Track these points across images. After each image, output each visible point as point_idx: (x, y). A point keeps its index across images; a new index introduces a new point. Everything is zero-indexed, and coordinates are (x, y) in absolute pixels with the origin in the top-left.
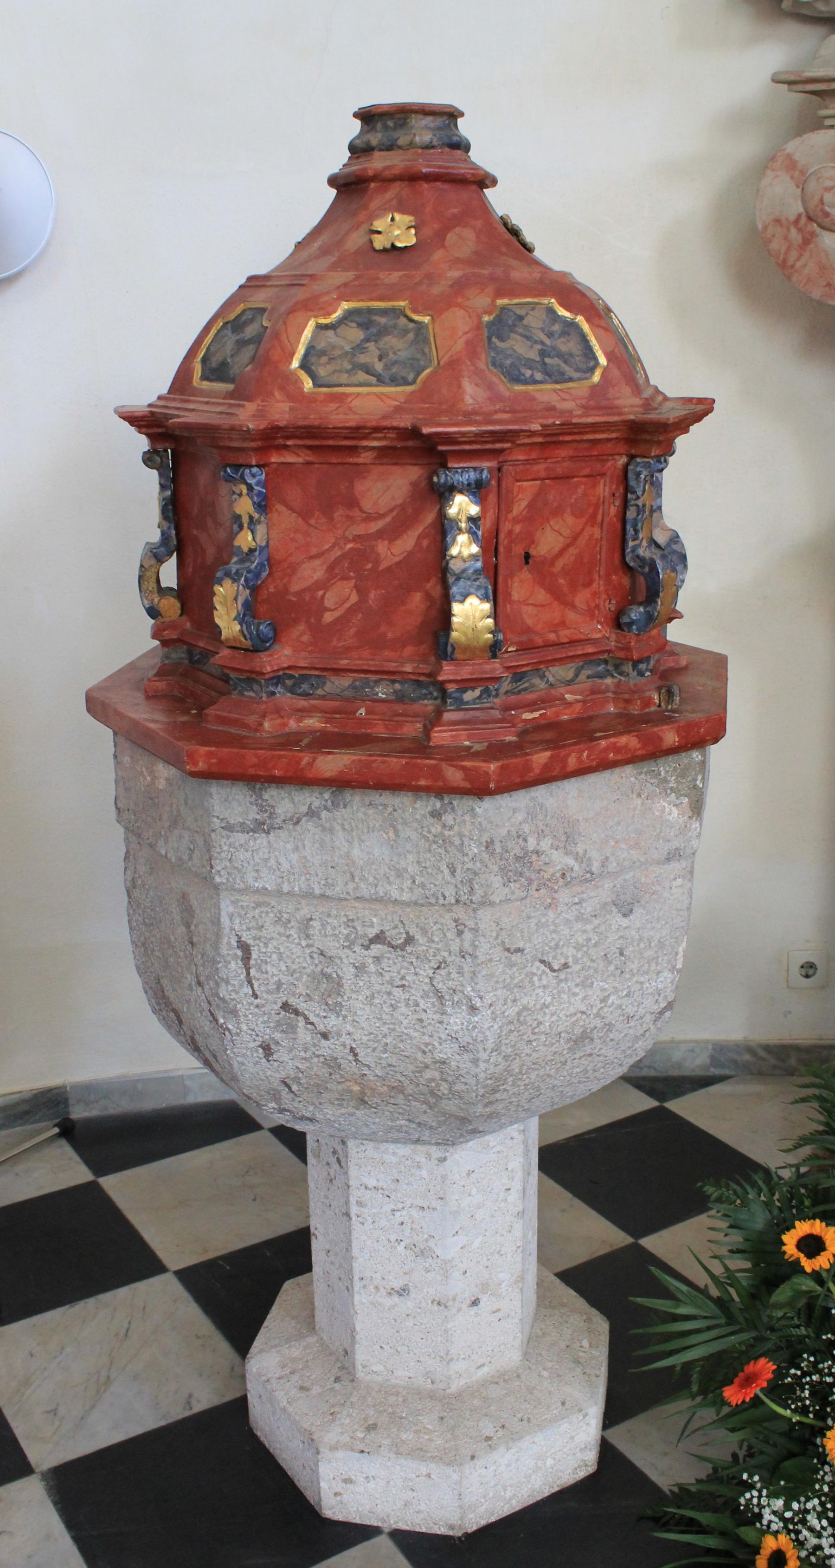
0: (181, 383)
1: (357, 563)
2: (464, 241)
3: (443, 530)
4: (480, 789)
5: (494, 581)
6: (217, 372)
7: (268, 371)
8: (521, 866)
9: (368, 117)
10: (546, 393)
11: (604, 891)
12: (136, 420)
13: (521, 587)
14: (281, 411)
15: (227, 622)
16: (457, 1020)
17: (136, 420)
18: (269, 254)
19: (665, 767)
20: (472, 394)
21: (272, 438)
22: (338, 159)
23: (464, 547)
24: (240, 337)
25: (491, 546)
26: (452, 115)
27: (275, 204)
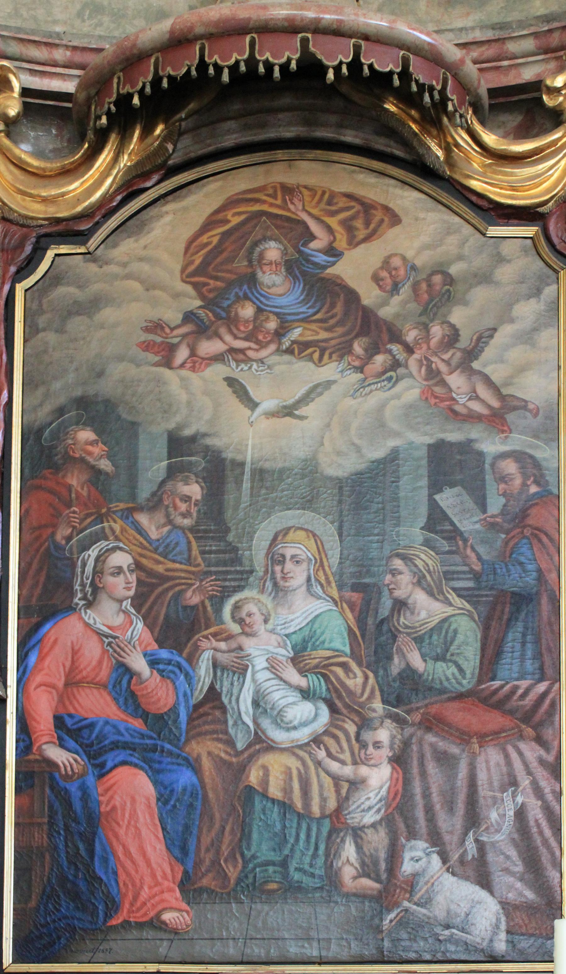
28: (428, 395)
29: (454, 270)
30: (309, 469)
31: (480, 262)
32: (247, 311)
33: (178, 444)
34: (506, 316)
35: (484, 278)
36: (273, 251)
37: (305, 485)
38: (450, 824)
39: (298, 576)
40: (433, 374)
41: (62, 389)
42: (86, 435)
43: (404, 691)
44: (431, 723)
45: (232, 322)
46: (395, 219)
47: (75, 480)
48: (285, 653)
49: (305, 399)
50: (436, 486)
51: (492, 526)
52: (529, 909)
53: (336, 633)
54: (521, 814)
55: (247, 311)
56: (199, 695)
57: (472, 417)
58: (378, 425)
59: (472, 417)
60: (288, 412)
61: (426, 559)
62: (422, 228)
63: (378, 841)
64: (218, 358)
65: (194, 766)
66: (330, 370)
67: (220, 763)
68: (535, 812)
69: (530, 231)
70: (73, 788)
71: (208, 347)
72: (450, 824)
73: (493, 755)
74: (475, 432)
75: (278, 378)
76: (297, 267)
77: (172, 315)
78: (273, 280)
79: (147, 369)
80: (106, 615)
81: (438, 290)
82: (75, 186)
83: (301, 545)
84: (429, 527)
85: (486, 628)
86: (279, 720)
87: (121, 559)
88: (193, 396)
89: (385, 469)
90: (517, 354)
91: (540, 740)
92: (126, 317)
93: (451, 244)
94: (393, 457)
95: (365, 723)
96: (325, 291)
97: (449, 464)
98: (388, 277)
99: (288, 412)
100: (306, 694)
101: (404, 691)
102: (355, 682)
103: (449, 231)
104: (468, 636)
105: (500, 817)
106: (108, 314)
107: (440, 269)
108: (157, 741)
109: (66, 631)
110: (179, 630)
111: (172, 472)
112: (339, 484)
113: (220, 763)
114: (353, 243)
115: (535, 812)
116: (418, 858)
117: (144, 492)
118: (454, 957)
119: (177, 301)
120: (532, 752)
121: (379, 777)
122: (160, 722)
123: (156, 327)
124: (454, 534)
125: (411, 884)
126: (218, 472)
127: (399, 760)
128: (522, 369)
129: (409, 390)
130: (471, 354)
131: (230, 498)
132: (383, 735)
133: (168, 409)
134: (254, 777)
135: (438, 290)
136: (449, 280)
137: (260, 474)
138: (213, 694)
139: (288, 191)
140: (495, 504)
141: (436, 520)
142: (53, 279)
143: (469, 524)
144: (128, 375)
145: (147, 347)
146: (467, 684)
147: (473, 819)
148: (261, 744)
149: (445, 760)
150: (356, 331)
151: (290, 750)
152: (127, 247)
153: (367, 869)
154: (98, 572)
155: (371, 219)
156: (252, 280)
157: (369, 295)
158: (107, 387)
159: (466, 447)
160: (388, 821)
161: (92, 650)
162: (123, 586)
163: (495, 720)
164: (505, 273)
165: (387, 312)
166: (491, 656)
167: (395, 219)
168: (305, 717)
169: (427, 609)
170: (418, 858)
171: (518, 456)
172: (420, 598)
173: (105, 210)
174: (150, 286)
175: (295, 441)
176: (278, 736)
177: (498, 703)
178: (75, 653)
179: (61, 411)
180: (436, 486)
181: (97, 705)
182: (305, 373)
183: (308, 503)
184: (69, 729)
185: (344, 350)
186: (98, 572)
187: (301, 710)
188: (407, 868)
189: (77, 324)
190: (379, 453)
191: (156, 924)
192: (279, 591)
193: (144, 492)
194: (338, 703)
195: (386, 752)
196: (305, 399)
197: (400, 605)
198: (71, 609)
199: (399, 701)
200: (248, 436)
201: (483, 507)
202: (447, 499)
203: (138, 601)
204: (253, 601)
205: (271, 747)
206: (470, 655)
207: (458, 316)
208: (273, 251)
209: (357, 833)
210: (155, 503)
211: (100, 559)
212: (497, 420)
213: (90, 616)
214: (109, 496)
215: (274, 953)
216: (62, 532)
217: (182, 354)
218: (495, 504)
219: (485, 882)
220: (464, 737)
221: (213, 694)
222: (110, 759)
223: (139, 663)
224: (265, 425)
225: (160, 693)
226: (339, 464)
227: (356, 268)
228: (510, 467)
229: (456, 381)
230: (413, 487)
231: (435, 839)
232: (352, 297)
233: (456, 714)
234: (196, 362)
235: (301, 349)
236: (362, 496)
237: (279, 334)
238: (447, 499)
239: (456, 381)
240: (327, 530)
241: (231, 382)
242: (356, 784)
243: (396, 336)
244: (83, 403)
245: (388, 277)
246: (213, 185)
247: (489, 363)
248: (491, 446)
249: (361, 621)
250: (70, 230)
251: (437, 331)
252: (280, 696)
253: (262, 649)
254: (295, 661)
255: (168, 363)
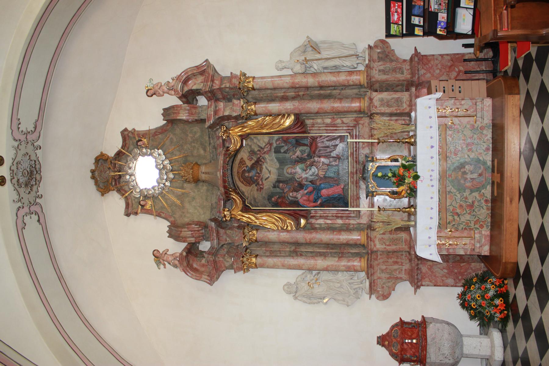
0: (397, 360)
1: (411, 349)
2: (387, 338)
3: (408, 342)
4: (426, 342)
5: (412, 339)
6: (396, 357)
7: (397, 354)
8: (434, 339)
9: (378, 344)
10: (399, 334)
11: (437, 331)
12: (423, 316)
13: (413, 337)
14: (399, 353)
15: (415, 359)
16: (446, 344)
17: (423, 316)
18: (387, 353)
19: (427, 326)
20: (399, 340)
21: (401, 354)
22: (380, 346)
23: (410, 341)
24: (393, 355)
25: (410, 339)
26: (378, 337)
27: (383, 352)
28: (267, 154)
29: (249, 150)
30: (278, 169)
31: (248, 147)
32: (255, 178)
33: (274, 187)
34: (256, 144)
35: (250, 146)
36: (247, 174)
37: (280, 169)
38: (329, 150)
39: (293, 171)
40: (264, 153)
41: (266, 202)
42: (273, 199)
43: (310, 156)
44: (314, 152)
45: (257, 180)
46: (242, 158)
47: (280, 200)
48: (304, 172)
49: (268, 170)
50: (280, 152)
51: (286, 145)
52: (341, 140)
53: (302, 166)
54: (327, 141)
55: (255, 178)
56: (310, 183)
57: (271, 148)
58: (272, 160)
59: (271, 148)
60: (270, 172)
61: (291, 154)
62: (244, 155)
63: (331, 159)
64: (262, 182)
65: (320, 184)
66: (264, 167)
67: (320, 181)
68: (327, 139)
69: (244, 141)
70: (324, 200)
71: (260, 183)
72: (329, 150)
73: (319, 144)
74: (273, 148)
75: (265, 173)
76: (249, 171)
77: (256, 188)
78: (251, 175)
79: (264, 191)
80: (299, 196)
81: (252, 152)
82: (238, 201)
83: (288, 170)
84: (286, 153)
85: (301, 146)
86: (314, 173)
87: (291, 194)
88: (267, 185)
89: (278, 159)
90: (261, 142)
91: (317, 138)
92: (256, 194)
93: (246, 151)
94: (276, 158)
95: (314, 162)
96: (253, 167)
97: (277, 151)
98: (251, 159)
99: (270, 172)
100: (310, 169)
101: (310, 156)
102: (309, 163)
103: (244, 151)
104: (301, 148)
105: (328, 143)
106: (256, 196)
107: (249, 152)
108: (317, 189)
109: (301, 201)
110: (301, 186)
111: (278, 187)
112: (280, 165)
113: (320, 181)
114: (245, 164)
115: (327, 139)
116: (333, 154)
117: (281, 191)
118: (401, 29)
119: (254, 187)
120: (318, 139)
121: (322, 159)
122: (314, 189)
123: (257, 190)
124: (287, 150)
125: (337, 155)
126: (279, 181)
127: (320, 157)
128: (264, 141)
129: (267, 156)
130: (261, 148)
131: (282, 180)
132: (316, 159)
133: (269, 188)
134: (322, 176)
135: (252, 152)
136: (251, 151)
137: (279, 176)
138: (310, 182)
139: (238, 173)
140: (283, 144)
141: (285, 152)
142: (251, 204)
143: (286, 148)
144: (264, 193)
145: (260, 191)
146: (309, 148)
147: (328, 147)
148: (317, 175)
149: (320, 151)
150: (258, 163)
151: (318, 171)
152: (246, 194)
153: (335, 161)
154: (293, 197)
155: (242, 162)
156: (251, 177)
157: (253, 162)
158: (266, 197)
159: (275, 149)
160: (328, 158)
161: (305, 198)
162: (295, 194)
163: (314, 144)
164: (250, 143)
165: (255, 159)
166: (305, 145)
167: (242, 158)
168: (314, 169)
169: (298, 153)
170: (333, 154)
171: (276, 141)
172: (296, 154)
173: (241, 197)
174: (252, 191)
175: (274, 170)
176: (316, 173)
177: (311, 144)
178: (304, 200)
179: (270, 203)
180: (280, 152)
181: (312, 197)
182: (264, 170)
183: (283, 169)
184: (315, 201)
185: (261, 165)
186: (293, 197)
187: (313, 170)
188: (335, 156)
189: (257, 201)
190: (276, 160)
191: (343, 189)
192: (295, 173)
193: (281, 191)
194: (312, 165)
195: (319, 159)
196: (268, 170)
197: (297, 157)
198: (298, 201)
199: (311, 157)
200: (273, 177)
201: (283, 146)
202: (282, 151)
203: (297, 192)
204: (297, 176)
205: (318, 174)
206: (305, 148)
207: (256, 150)
208: (247, 174)
209: (330, 162)
210: (283, 190)
211: (291, 197)
212: (271, 145)
213: (299, 198)
214: (282, 196)
215: (320, 62)
216: (287, 202)
217: (261, 186)
218: (283, 144)
219: (337, 145)
220: (316, 148)
221: (310, 182)
222: (320, 195)
223: (306, 191)
224: (272, 175)
225: (310, 189)
226: (278, 165)
227: (249, 163)
228: (278, 143)
229: (265, 150)
230: (280, 156)
231: (331, 152)
232: (253, 164)
233: (313, 149)
234: (263, 184)
235: (261, 171)
236: (282, 162)
237: (258, 173)
238: (282, 151)
239: (265, 150)
240: (287, 167)
241: (265, 180)
242: (323, 163)
243: (259, 158)
244: (268, 200)
245: (251, 159)
246: (237, 183)
247: (263, 145)
248: (275, 145)
249: (300, 162)
250: (244, 202)
251: (258, 153)
252: (311, 173)
253: (304, 176)
254: (306, 171)
255: (263, 188)
